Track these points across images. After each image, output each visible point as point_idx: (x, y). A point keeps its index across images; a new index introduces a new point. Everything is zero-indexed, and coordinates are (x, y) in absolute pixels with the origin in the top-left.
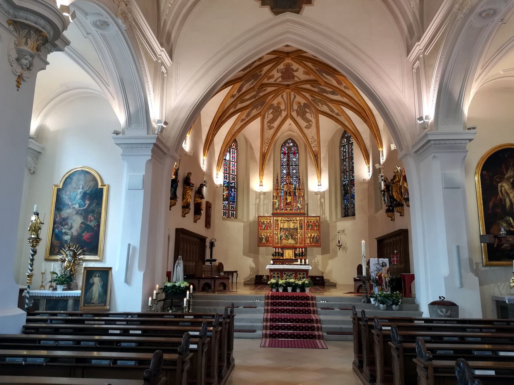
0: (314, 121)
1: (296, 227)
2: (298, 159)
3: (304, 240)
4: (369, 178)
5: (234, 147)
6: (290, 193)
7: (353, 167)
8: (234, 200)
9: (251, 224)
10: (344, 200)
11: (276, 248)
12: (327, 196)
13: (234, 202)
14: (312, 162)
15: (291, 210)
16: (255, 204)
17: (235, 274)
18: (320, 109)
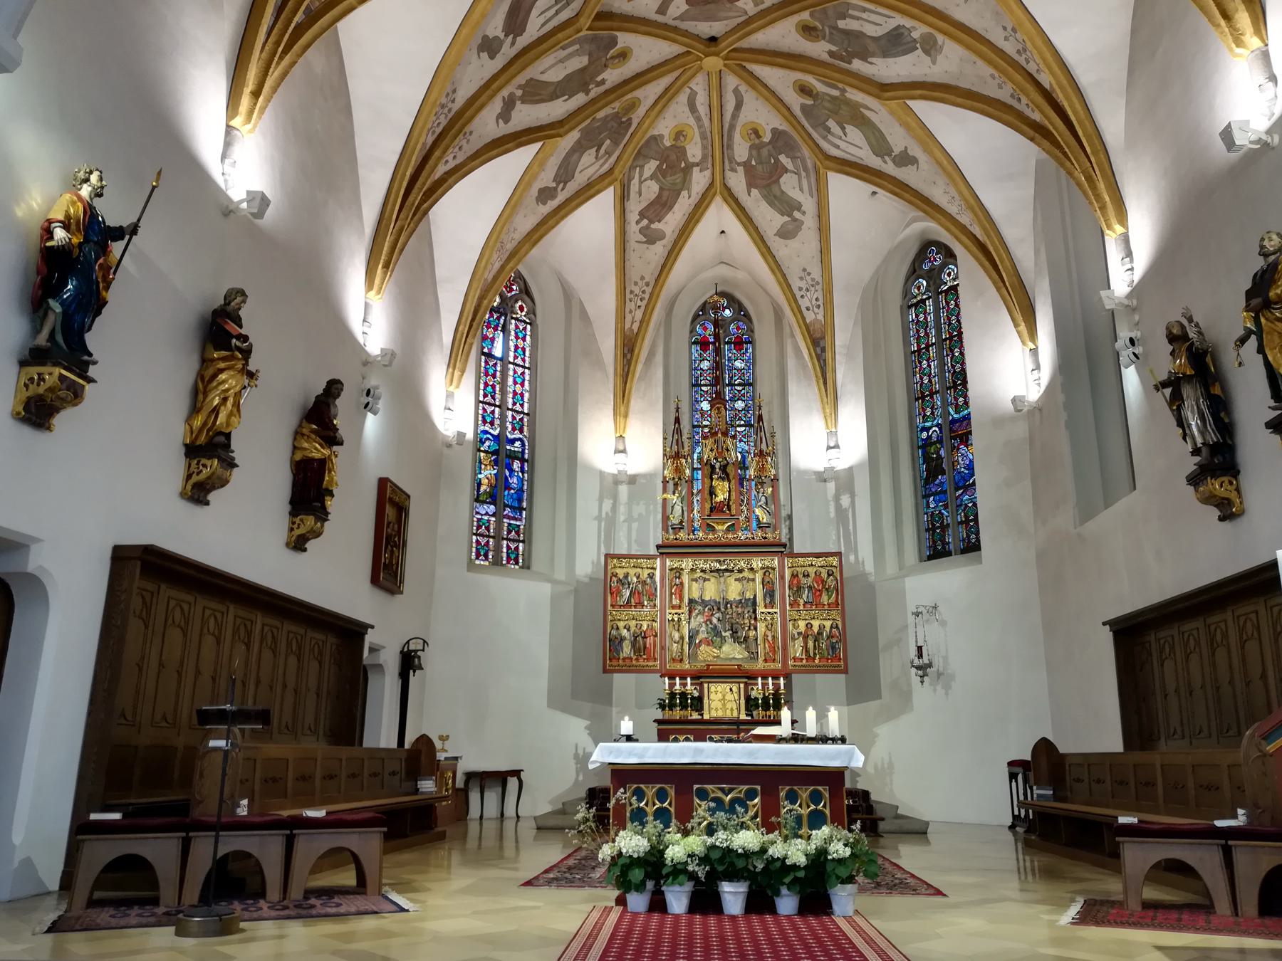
0: (809, 204)
1: (749, 595)
2: (752, 363)
3: (779, 646)
4: (1034, 394)
5: (522, 315)
6: (724, 468)
7: (963, 371)
8: (520, 500)
9: (579, 590)
10: (926, 496)
11: (672, 677)
12: (862, 484)
13: (521, 509)
14: (805, 366)
15: (728, 530)
16: (599, 518)
17: (512, 783)
18: (834, 152)
